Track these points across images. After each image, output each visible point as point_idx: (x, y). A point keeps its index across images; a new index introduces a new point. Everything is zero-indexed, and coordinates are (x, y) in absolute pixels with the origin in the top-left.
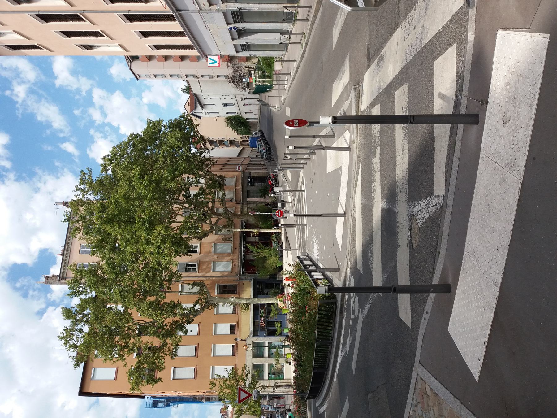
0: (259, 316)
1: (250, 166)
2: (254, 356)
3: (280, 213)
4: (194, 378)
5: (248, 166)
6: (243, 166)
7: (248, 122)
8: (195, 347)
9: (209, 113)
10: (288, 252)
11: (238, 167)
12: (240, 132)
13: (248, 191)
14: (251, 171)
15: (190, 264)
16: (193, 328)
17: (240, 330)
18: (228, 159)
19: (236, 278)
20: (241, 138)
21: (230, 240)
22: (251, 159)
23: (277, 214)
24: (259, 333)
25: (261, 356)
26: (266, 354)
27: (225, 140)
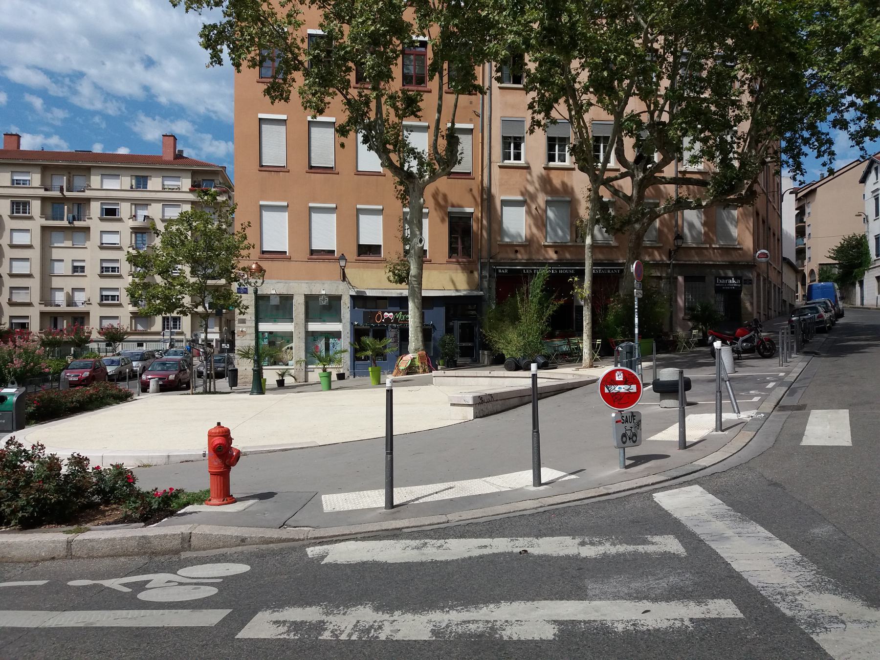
0: (398, 309)
1: (764, 284)
2: (310, 299)
3: (623, 389)
4: (262, 166)
5: (764, 279)
6: (764, 267)
7: (854, 285)
8: (332, 165)
9: (877, 199)
10: (471, 409)
11: (766, 251)
12: (825, 269)
13: (702, 279)
14: (755, 285)
15: (522, 145)
16: (369, 160)
17: (368, 267)
18: (778, 236)
19: (485, 254)
20: (812, 271)
21: (577, 237)
22: (779, 288)
23: (619, 377)
24: (360, 311)
25: (309, 317)
26: (314, 327)
27: (805, 241)
